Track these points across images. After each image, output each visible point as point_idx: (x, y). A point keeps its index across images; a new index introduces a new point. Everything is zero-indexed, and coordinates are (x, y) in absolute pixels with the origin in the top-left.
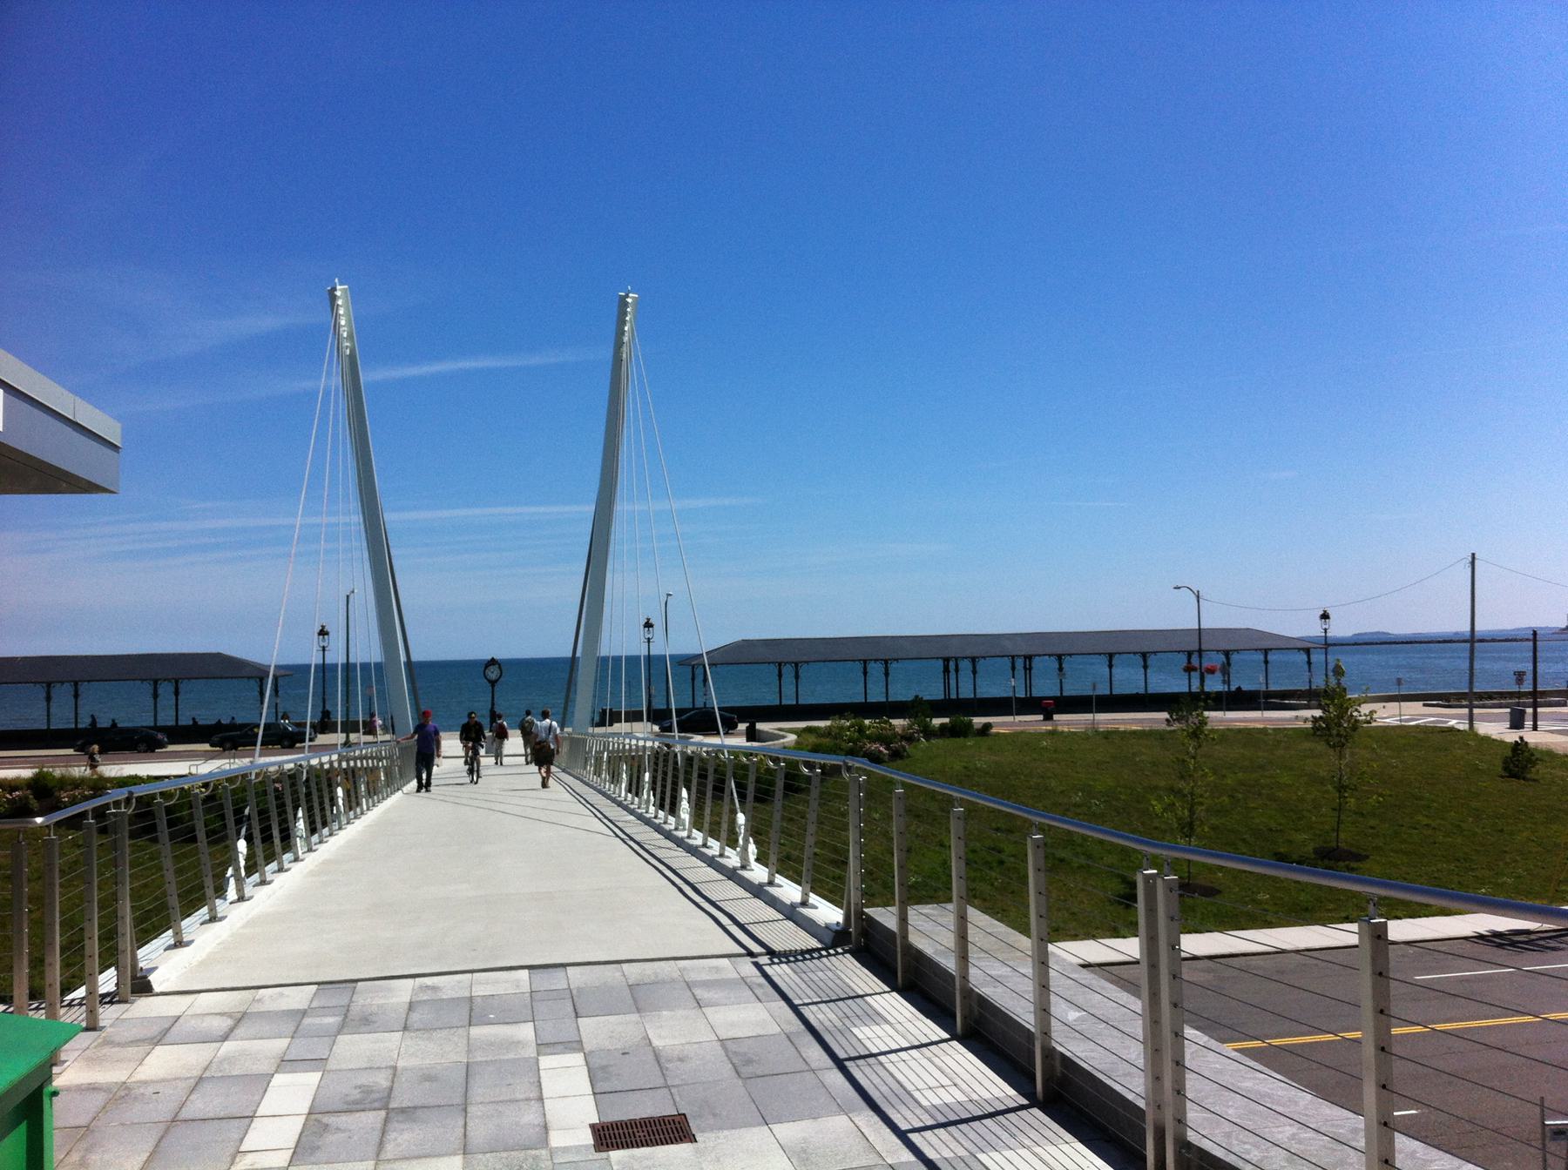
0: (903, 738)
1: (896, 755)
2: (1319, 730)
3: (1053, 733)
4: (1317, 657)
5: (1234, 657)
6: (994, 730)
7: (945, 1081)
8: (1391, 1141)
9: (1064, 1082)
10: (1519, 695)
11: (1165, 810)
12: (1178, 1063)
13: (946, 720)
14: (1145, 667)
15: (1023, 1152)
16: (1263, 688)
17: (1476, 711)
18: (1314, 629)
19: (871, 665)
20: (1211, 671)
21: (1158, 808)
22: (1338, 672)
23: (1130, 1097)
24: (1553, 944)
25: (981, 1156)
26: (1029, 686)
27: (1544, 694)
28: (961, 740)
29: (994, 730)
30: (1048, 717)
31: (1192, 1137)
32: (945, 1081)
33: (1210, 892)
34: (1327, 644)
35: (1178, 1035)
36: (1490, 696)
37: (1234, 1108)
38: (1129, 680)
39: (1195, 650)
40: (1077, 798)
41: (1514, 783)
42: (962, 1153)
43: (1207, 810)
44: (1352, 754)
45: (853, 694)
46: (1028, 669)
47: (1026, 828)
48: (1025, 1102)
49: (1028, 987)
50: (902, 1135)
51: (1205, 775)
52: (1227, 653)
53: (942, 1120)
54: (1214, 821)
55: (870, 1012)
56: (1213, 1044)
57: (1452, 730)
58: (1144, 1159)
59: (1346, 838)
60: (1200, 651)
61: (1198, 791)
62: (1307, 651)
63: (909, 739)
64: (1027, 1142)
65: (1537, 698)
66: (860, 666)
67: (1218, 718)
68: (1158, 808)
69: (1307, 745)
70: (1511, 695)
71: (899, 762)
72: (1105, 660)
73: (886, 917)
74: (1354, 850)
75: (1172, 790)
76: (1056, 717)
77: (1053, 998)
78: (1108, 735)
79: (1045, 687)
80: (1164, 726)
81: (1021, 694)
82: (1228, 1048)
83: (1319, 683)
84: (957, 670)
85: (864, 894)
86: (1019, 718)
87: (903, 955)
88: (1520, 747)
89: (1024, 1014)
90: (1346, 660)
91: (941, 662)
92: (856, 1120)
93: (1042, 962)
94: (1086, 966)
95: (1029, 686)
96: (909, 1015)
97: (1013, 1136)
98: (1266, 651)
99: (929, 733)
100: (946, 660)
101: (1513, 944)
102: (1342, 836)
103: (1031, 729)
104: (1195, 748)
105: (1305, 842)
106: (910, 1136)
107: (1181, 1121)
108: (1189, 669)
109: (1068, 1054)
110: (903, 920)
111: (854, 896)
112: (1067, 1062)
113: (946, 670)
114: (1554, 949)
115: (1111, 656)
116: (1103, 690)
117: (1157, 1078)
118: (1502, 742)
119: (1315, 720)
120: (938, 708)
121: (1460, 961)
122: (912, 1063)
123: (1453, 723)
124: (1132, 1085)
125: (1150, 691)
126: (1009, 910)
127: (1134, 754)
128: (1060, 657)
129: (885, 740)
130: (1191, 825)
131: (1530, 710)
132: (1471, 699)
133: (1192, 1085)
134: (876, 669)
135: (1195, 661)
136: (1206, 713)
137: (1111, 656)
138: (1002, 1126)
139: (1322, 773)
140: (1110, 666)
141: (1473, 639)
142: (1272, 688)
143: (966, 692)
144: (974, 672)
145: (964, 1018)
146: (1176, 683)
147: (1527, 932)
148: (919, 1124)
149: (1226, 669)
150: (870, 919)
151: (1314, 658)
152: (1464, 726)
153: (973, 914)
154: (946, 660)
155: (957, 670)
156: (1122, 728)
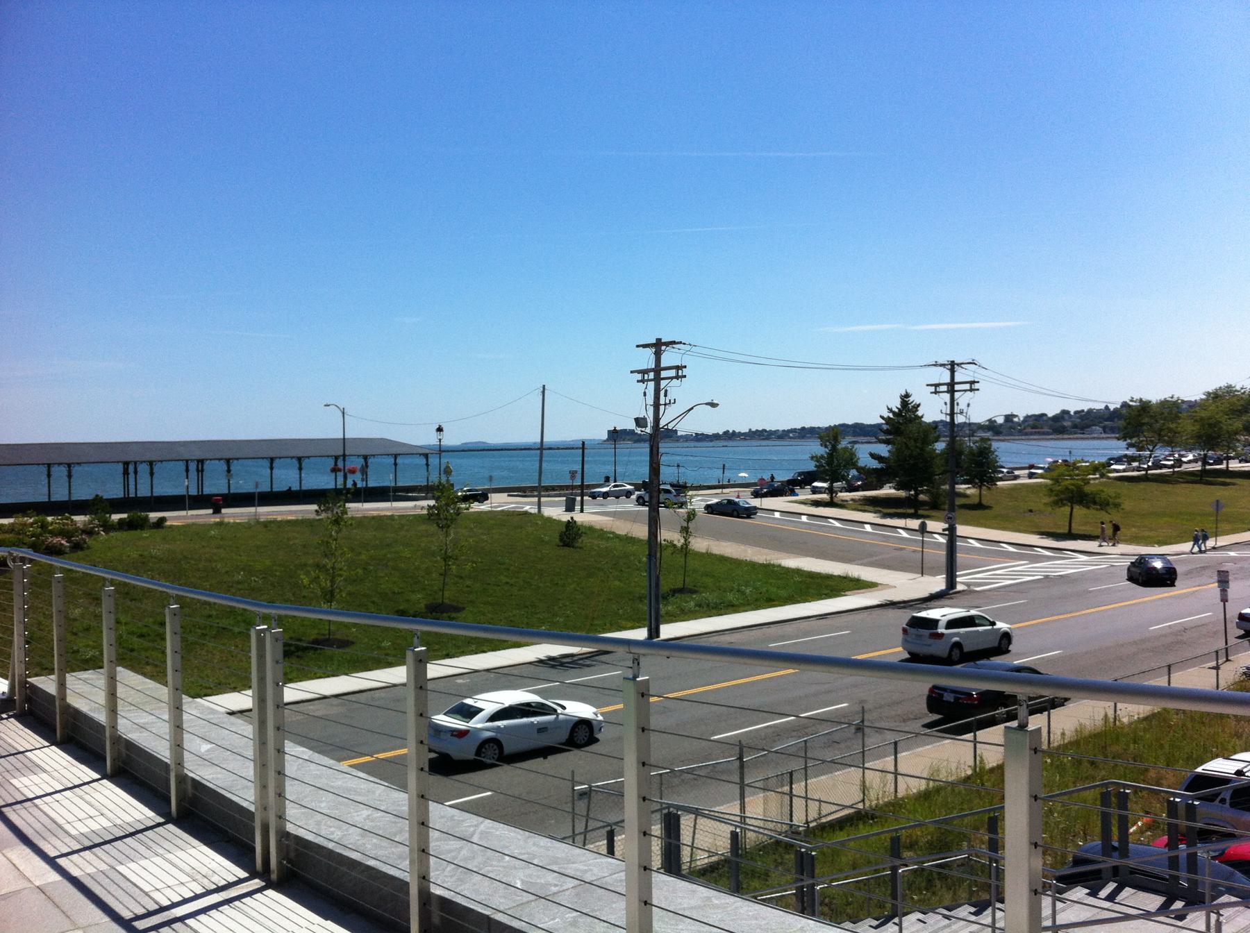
0: (84, 532)
1: (77, 547)
2: (432, 516)
3: (220, 524)
4: (434, 461)
5: (370, 461)
6: (168, 523)
7: (93, 812)
8: (427, 808)
9: (195, 801)
10: (573, 487)
11: (311, 582)
12: (279, 773)
13: (125, 516)
14: (300, 469)
15: (157, 860)
16: (393, 484)
17: (543, 499)
18: (430, 439)
19: (54, 469)
20: (353, 471)
21: (306, 581)
22: (448, 471)
23: (245, 804)
24: (588, 662)
25: (121, 868)
26: (200, 484)
27: (589, 487)
28: (137, 533)
29: (168, 523)
30: (217, 511)
31: (290, 828)
32: (93, 812)
33: (344, 644)
34: (441, 451)
35: (280, 751)
36: (553, 488)
37: (324, 803)
38: (286, 478)
39: (340, 455)
40: (240, 576)
41: (567, 550)
42: (103, 867)
43: (345, 580)
44: (456, 533)
45: (38, 494)
46: (200, 471)
47: (164, 599)
48: (162, 820)
49: (165, 729)
50: (52, 862)
51: (343, 554)
52: (366, 458)
53: (88, 843)
54: (350, 588)
55: (30, 764)
56: (331, 762)
57: (526, 513)
58: (254, 849)
59: (449, 596)
60: (344, 456)
61: (338, 566)
62: (426, 456)
63: (89, 532)
64: (161, 851)
65: (584, 489)
66: (44, 469)
67: (357, 509)
68: (306, 581)
69: (423, 527)
70: (567, 487)
71: (80, 553)
72: (267, 463)
73: (47, 684)
74: (455, 604)
75: (318, 566)
76: (224, 511)
77: (186, 736)
78: (267, 524)
79: (215, 485)
80: (313, 516)
81: (193, 492)
82: (344, 766)
83: (434, 479)
84: (136, 472)
85: (28, 666)
86: (191, 512)
87: (62, 714)
88: (571, 524)
89: (162, 750)
90: (453, 462)
91: (121, 465)
92: (9, 855)
93: (177, 709)
94: (232, 713)
95: (200, 484)
96: (65, 764)
97: (149, 848)
98: (396, 456)
99: (108, 527)
100: (126, 464)
101: (562, 664)
102: (447, 594)
103: (200, 521)
104: (337, 532)
105: (419, 600)
106: (58, 860)
107: (281, 817)
108: (335, 470)
109: (197, 778)
110: (62, 685)
111: (18, 669)
112: (197, 785)
113: (126, 473)
114: (588, 666)
115: (272, 460)
116: (265, 487)
117: (264, 787)
118: (560, 522)
119: (430, 508)
120: (117, 505)
121: (526, 681)
122: (65, 802)
123: (527, 508)
124: (245, 795)
125: (304, 488)
126: (153, 669)
127: (289, 539)
128: (228, 461)
129: (66, 534)
130: (332, 593)
131: (579, 498)
132: (539, 491)
133: (291, 790)
134: (60, 472)
135: (340, 464)
136: (348, 505)
137: (272, 460)
138: (141, 842)
139: (433, 548)
140: (272, 468)
141: (542, 448)
142: (400, 484)
143: (144, 491)
144: (152, 474)
145: (113, 760)
146: (322, 480)
147: (572, 655)
148: (65, 850)
149: (364, 470)
150: (33, 686)
151: (430, 460)
152: (534, 510)
153: (123, 674)
154: (126, 464)
155: (136, 472)
156: (279, 518)
